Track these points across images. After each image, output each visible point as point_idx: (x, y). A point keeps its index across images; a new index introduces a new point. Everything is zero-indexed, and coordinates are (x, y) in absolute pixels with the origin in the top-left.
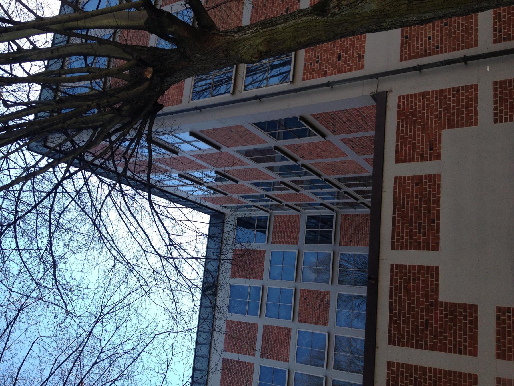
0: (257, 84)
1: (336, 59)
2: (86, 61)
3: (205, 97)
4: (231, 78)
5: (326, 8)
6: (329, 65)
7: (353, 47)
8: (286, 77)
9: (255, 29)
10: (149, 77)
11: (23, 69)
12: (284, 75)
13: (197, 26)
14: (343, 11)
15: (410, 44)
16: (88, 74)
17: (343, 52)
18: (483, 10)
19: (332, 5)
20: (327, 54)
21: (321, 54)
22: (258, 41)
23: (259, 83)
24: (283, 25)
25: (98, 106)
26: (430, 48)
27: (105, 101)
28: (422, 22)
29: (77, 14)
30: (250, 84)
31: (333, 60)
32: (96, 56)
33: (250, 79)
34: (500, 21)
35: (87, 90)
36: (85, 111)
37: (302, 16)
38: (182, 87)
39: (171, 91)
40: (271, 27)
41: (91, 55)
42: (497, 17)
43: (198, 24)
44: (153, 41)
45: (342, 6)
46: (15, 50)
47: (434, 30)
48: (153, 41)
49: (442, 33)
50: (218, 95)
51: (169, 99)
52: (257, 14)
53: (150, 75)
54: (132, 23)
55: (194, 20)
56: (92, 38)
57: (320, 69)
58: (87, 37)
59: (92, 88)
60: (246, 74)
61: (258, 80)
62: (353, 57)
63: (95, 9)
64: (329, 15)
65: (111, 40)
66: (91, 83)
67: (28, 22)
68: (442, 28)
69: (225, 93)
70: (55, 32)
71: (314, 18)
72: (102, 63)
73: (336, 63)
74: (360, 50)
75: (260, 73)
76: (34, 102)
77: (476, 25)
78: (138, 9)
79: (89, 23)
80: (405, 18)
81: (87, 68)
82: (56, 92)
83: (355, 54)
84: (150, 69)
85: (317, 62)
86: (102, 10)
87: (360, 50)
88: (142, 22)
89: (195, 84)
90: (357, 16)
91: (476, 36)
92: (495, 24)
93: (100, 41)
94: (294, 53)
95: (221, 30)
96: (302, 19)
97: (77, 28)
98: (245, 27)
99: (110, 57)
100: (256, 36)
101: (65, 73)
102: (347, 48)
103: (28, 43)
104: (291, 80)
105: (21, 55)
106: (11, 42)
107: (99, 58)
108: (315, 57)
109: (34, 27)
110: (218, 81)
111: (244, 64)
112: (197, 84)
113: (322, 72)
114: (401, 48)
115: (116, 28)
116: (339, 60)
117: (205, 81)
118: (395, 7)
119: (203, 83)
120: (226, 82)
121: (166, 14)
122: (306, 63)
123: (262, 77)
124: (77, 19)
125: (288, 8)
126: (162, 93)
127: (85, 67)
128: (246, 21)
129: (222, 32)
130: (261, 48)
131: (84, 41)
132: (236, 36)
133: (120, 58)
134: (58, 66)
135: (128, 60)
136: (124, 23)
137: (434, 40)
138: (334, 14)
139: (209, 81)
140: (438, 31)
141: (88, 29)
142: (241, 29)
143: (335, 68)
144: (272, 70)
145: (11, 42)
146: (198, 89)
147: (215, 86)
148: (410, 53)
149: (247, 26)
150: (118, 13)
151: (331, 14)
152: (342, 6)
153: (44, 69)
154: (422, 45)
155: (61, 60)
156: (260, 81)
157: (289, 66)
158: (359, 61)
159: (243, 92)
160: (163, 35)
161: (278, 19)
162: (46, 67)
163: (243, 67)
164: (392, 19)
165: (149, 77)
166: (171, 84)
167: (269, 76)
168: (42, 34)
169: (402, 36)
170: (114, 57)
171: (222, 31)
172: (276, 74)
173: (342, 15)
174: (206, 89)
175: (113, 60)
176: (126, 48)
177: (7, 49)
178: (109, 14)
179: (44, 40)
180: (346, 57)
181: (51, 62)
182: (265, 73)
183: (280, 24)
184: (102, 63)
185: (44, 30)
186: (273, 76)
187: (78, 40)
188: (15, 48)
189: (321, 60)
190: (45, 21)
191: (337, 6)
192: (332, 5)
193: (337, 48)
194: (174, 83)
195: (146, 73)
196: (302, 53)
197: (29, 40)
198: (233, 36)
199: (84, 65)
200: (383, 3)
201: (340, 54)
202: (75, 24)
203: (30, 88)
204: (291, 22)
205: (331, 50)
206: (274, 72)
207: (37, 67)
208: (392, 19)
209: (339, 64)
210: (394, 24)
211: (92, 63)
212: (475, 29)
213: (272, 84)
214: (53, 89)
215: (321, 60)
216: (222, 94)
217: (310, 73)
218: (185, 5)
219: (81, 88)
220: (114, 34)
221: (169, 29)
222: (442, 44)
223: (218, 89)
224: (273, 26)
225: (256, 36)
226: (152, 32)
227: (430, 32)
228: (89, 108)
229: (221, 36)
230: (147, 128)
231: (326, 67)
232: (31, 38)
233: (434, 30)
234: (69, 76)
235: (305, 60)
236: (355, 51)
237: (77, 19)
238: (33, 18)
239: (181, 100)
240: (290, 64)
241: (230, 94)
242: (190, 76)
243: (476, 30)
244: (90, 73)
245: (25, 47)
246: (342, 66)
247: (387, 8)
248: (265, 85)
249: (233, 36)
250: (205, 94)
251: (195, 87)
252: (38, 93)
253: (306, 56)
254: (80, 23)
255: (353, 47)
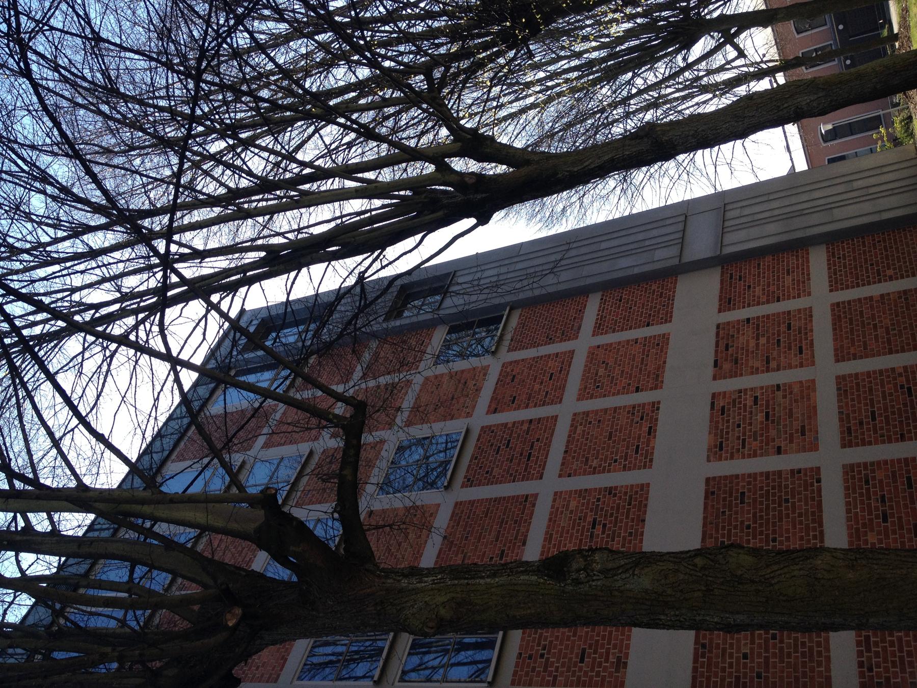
0: (427, 672)
1: (577, 657)
2: (132, 572)
3: (324, 679)
4: (381, 650)
5: (565, 569)
6: (563, 666)
7: (609, 644)
8: (482, 671)
9: (439, 577)
10: (230, 624)
11: (18, 562)
12: (480, 666)
13: (342, 551)
14: (593, 581)
15: (710, 659)
16: (125, 595)
17: (590, 648)
18: (836, 628)
19: (575, 566)
20: (561, 644)
21: (551, 642)
22: (443, 599)
23: (430, 671)
24: (489, 580)
25: (121, 660)
26: (745, 674)
27: (137, 652)
28: (730, 628)
29: (148, 494)
30: (413, 670)
31: (571, 659)
32: (152, 567)
33: (415, 660)
34: (868, 650)
35: (113, 624)
36: (95, 665)
37: (522, 572)
38: (288, 652)
39: (267, 655)
40: (467, 579)
41: (144, 564)
42: (864, 645)
43: (344, 549)
44: (261, 562)
45: (592, 570)
46: (19, 529)
47: (753, 642)
48: (261, 562)
49: (767, 651)
50: (350, 678)
51: (257, 669)
52: (449, 550)
53: (234, 621)
54: (234, 526)
55: (339, 542)
56: (157, 536)
57: (545, 671)
58: (150, 533)
59: (123, 622)
60: (411, 649)
61: (431, 664)
62: (607, 661)
63: (180, 491)
64: (569, 581)
65: (189, 545)
66: (125, 615)
67: (58, 490)
68: (766, 640)
69: (364, 677)
70: (99, 514)
71: (542, 581)
72: (160, 581)
73: (575, 666)
74: (621, 652)
75: (436, 652)
76: (10, 625)
77: (828, 649)
78: (251, 505)
79: (161, 511)
80: (699, 615)
81: (130, 586)
82: (57, 617)
83: (611, 656)
84: (238, 611)
85: (542, 656)
86: (192, 495)
87: (621, 652)
88: (251, 527)
89: (313, 647)
90: (616, 593)
91: (828, 669)
92: (860, 654)
93: (168, 543)
94: (501, 633)
95: (382, 566)
96: (522, 578)
97: (137, 516)
98: (422, 569)
99: (175, 574)
100: (439, 590)
101: (88, 586)
102: (597, 641)
103: (47, 523)
104: (490, 679)
105: (25, 538)
106: (18, 515)
107: (155, 572)
108: (539, 645)
109: (66, 500)
110: (356, 652)
111: (407, 634)
112: (316, 650)
113: (549, 676)
114: (694, 663)
115: (204, 529)
116: (582, 661)
117: (332, 647)
118: (681, 591)
119: (329, 650)
120: (371, 656)
121: (294, 523)
122: (520, 654)
123: (438, 660)
124: (143, 502)
125: (503, 551)
126: (245, 656)
127: (127, 582)
128: (428, 560)
129: (383, 570)
130: (442, 612)
131: (142, 538)
132: (404, 582)
133: (192, 580)
134: (83, 568)
135: (205, 586)
136: (220, 524)
137: (752, 661)
138: (577, 582)
139: (339, 649)
140: (760, 645)
141: (156, 520)
142: (415, 572)
143: (573, 676)
144: (458, 651)
145: (18, 515)
146: (315, 660)
147: (348, 661)
148: (710, 676)
149: (427, 569)
150: (217, 505)
151: (573, 580)
152: (592, 570)
153: (54, 570)
154: (731, 666)
155: (89, 561)
156: (433, 668)
157: (491, 651)
158: (617, 671)
159: (397, 684)
160: (279, 557)
161: (482, 569)
162: (60, 567)
163: (406, 640)
164: (677, 613)
165: (230, 624)
166: (267, 645)
167: (453, 661)
168: (78, 512)
169: (696, 643)
170: (184, 577)
171: (383, 568)
172: (465, 661)
173: (590, 586)
174: (331, 662)
175: (180, 580)
176: (210, 567)
177: (7, 524)
178: (200, 505)
179: (74, 523)
180: (595, 658)
181: (71, 561)
182: (445, 655)
183: (482, 578)
184: (160, 581)
185: (81, 507)
186: (459, 664)
187: (132, 535)
188: (21, 523)
189: (549, 653)
190: (91, 494)
191: (585, 569)
192: (575, 566)
193: (580, 637)
194: (274, 643)
195: (228, 616)
196: (516, 636)
197: (50, 518)
198: (399, 581)
199: (126, 579)
200: (663, 581)
201: (584, 650)
202: (137, 508)
203: (15, 597)
204: (502, 579)
205: (568, 639)
206: (462, 656)
207: (41, 565)
208: (677, 613)
209: (581, 669)
210: (681, 622)
211: (141, 579)
212: (826, 657)
213: (454, 679)
214: (54, 611)
215: (549, 653)
216: (357, 678)
217: (527, 674)
218: (332, 514)
219: (104, 621)
220: (198, 538)
221: (292, 548)
222: (767, 671)
223: (352, 666)
224: (471, 579)
225: (439, 590)
226: (261, 547)
227: (746, 644)
228: (104, 659)
229: (379, 577)
230: (673, 96)
231: (557, 668)
232: (56, 517)
233: (753, 642)
234: (91, 592)
235: (521, 647)
236: (612, 651)
237: (143, 502)
238: (73, 484)
239: (278, 676)
240: (493, 649)
241: (372, 683)
242: (305, 636)
243: (828, 659)
244: (130, 596)
245: (39, 528)
246: (586, 673)
247: (669, 591)
248: (440, 678)
249: (399, 581)
250: (327, 670)
251: (312, 654)
252: (24, 611)
253: (523, 639)
254: (147, 509)
255: (609, 644)
